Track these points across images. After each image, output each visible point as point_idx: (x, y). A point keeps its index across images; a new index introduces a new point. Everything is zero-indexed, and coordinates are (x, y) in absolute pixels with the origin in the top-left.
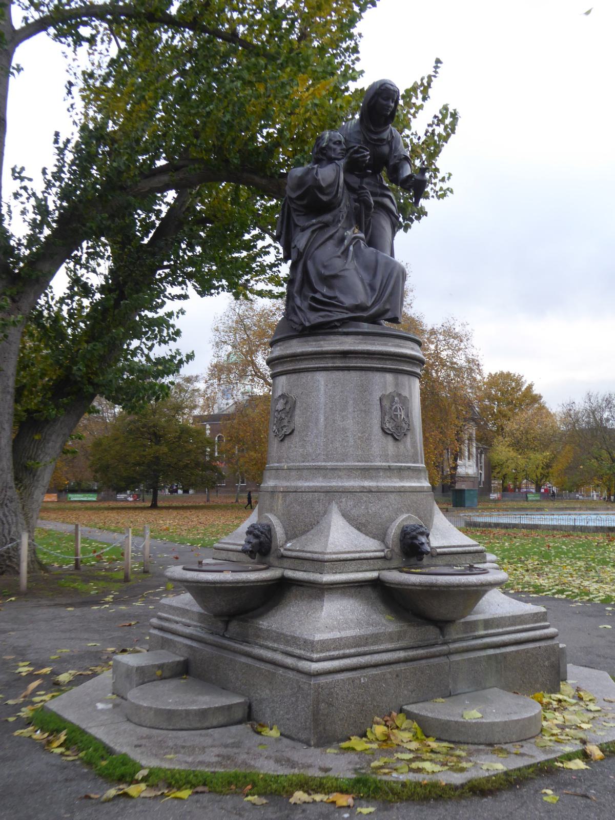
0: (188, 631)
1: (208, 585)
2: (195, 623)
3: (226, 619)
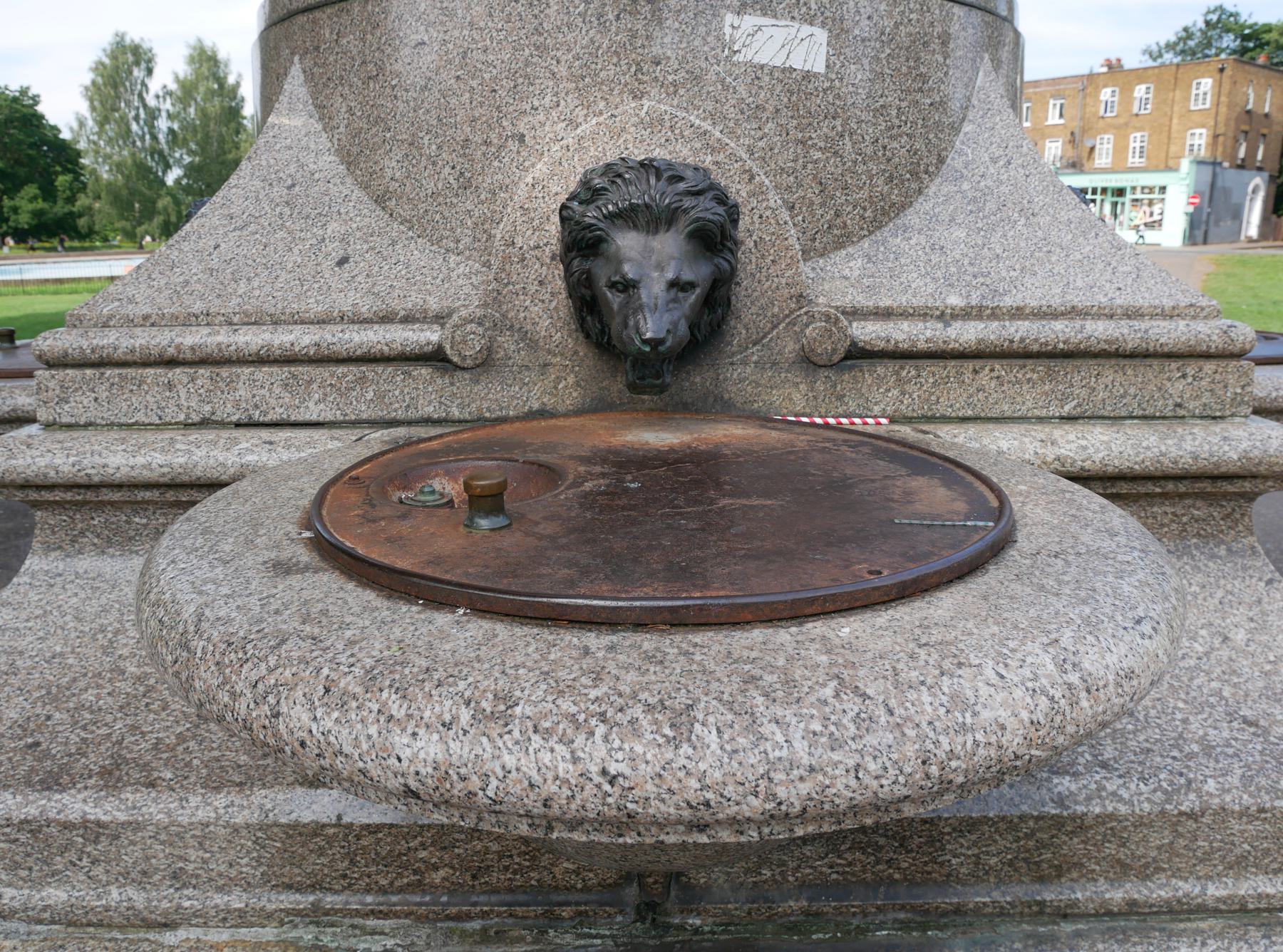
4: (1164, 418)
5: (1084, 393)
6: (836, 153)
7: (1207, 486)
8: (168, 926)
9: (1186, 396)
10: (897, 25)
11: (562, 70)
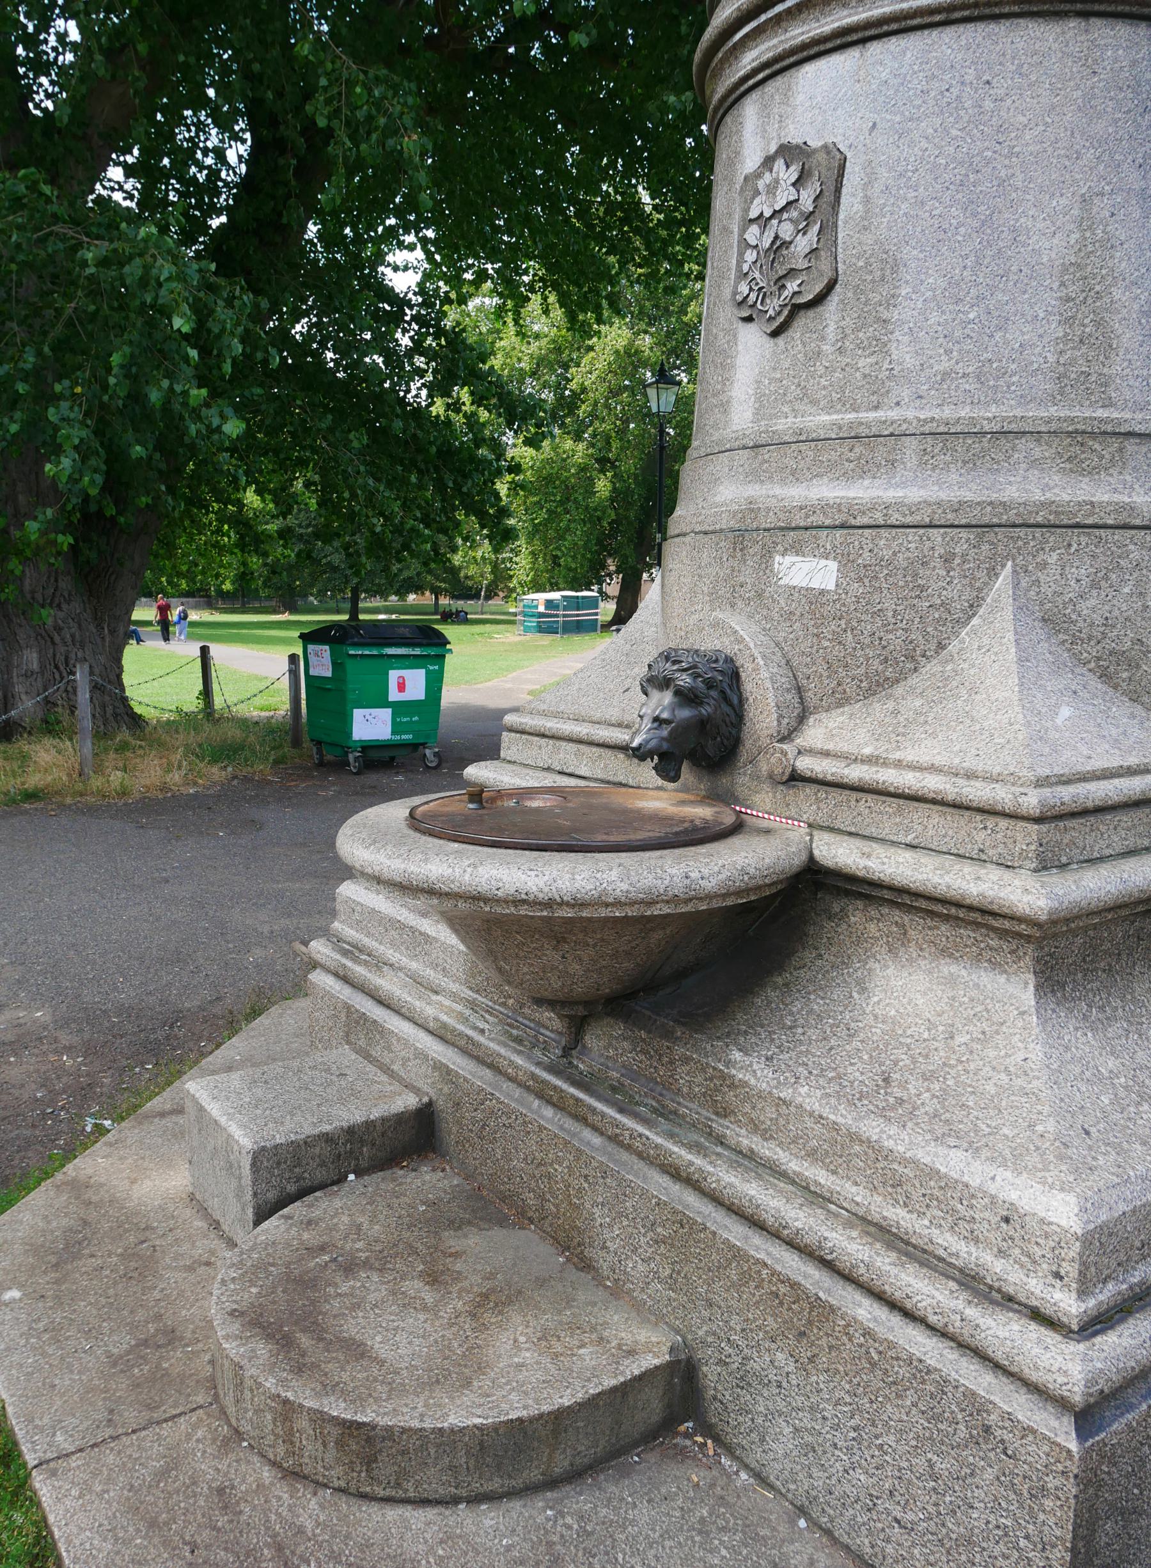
0: (429, 1010)
1: (524, 911)
2: (454, 987)
3: (581, 1011)
4: (972, 859)
5: (920, 828)
6: (840, 643)
7: (977, 916)
8: (436, 993)
9: (987, 844)
10: (895, 554)
11: (705, 589)
